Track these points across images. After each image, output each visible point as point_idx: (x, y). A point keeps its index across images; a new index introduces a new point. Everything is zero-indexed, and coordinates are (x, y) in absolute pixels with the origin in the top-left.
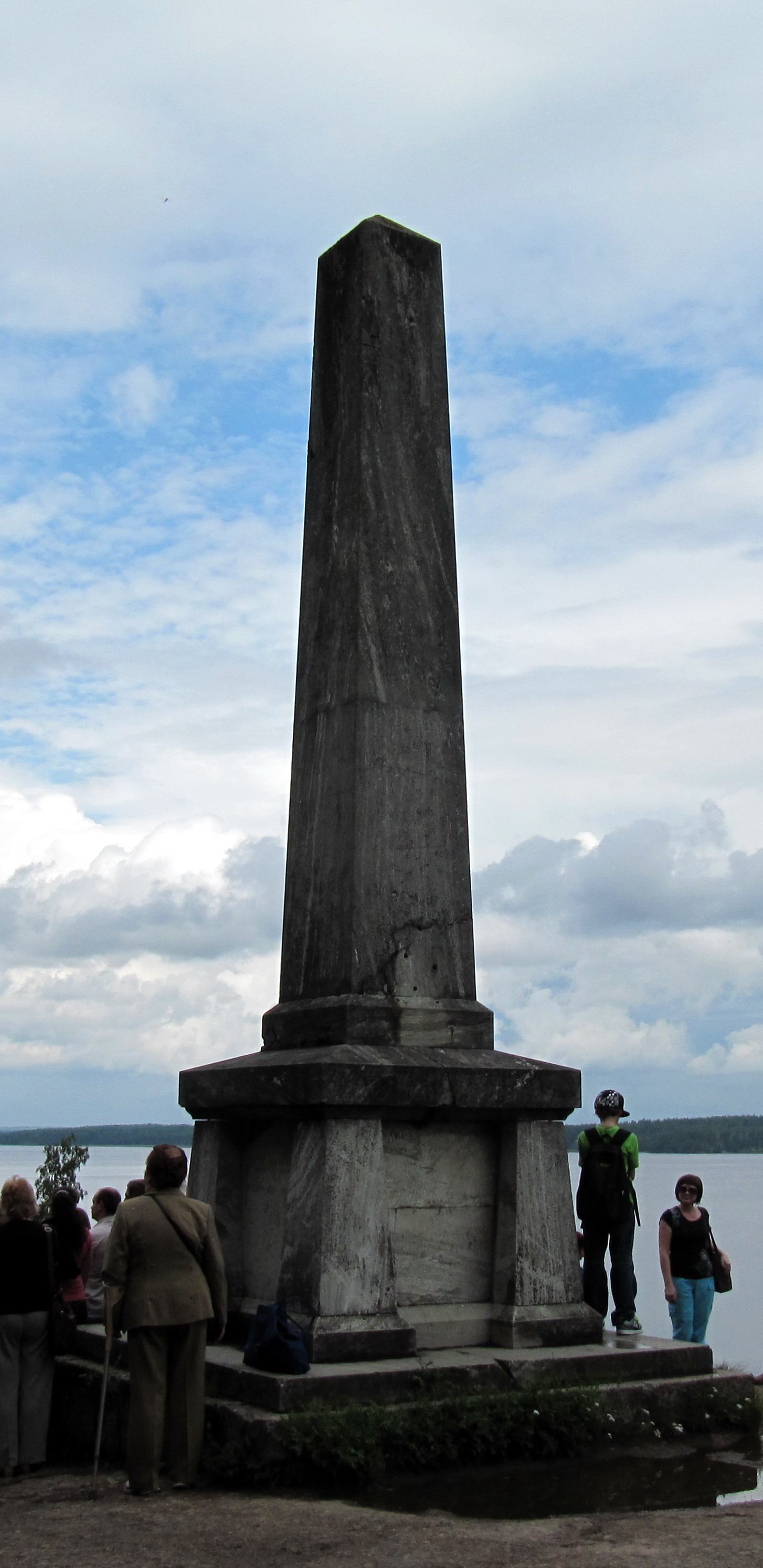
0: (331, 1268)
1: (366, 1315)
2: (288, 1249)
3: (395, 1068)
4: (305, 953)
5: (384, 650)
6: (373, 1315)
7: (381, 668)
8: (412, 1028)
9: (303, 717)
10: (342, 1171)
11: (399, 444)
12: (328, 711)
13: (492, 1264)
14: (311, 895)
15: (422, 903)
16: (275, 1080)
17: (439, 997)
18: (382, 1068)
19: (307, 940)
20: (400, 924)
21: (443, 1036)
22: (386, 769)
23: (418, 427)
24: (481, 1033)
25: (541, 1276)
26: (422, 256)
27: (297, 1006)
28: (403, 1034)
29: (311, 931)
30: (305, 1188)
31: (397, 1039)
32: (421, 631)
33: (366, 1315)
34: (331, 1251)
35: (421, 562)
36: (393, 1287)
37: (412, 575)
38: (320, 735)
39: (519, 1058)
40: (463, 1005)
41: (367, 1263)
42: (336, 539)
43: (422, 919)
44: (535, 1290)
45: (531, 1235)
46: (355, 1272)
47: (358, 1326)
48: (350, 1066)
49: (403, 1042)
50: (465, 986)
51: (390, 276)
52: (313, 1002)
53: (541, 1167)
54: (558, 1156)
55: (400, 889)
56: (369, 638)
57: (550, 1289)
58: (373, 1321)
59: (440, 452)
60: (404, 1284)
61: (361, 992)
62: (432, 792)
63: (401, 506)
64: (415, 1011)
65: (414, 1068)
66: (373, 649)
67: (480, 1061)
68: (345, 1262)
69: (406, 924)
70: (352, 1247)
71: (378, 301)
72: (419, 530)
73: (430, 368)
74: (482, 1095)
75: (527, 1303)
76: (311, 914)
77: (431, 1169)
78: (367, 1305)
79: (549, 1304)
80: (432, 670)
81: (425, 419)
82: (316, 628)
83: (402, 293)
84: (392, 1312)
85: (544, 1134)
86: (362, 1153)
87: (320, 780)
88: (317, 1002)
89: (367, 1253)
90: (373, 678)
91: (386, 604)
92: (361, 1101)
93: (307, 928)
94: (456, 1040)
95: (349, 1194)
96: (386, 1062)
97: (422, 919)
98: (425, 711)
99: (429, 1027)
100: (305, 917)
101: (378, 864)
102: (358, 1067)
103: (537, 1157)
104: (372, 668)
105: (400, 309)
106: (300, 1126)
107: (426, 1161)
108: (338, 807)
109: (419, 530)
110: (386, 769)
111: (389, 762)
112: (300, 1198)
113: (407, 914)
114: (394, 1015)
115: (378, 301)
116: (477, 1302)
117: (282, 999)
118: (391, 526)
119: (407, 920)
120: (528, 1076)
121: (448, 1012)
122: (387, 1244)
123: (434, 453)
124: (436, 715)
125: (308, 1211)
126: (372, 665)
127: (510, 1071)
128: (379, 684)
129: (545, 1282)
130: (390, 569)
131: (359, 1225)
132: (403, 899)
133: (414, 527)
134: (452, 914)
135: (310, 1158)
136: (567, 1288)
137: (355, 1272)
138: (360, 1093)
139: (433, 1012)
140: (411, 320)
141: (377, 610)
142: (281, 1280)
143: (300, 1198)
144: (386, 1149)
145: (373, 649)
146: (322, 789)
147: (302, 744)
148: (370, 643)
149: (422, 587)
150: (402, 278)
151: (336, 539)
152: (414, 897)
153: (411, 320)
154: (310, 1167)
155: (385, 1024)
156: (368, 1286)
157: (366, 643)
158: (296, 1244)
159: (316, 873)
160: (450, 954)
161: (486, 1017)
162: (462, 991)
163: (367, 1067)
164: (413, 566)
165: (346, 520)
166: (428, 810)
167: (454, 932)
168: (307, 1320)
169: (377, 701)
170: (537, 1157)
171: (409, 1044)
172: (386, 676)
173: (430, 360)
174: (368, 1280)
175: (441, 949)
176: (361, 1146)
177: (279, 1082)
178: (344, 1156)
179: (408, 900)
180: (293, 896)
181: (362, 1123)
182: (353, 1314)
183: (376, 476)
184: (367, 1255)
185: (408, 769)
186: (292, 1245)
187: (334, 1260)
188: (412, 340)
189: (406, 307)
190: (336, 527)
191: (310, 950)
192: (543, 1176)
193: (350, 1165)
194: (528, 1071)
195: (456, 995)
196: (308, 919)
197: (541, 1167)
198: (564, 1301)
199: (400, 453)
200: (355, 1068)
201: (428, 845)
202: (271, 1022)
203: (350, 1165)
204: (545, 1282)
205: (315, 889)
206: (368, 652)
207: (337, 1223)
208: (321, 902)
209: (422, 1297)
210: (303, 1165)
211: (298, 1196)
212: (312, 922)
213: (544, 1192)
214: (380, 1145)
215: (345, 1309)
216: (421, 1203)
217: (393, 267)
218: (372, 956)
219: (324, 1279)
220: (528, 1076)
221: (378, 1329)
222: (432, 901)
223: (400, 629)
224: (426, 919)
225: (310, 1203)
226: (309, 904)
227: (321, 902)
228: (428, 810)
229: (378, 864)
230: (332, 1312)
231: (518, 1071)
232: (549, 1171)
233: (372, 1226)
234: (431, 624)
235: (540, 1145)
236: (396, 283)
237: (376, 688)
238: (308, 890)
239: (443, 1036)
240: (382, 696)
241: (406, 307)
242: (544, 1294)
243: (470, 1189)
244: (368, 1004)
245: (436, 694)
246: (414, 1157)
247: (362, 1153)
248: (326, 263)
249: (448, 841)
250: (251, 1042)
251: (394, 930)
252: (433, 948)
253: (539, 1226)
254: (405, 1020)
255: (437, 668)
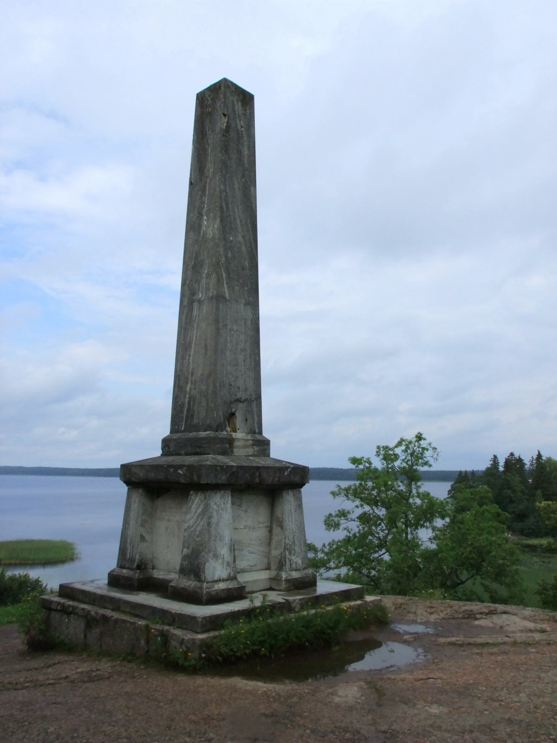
0: (210, 559)
1: (224, 580)
2: (185, 550)
3: (238, 466)
4: (185, 412)
5: (228, 276)
6: (227, 580)
7: (227, 283)
8: (238, 447)
9: (185, 303)
10: (215, 514)
11: (236, 182)
12: (199, 301)
13: (269, 552)
14: (189, 385)
15: (242, 391)
16: (179, 471)
17: (249, 433)
18: (232, 466)
19: (186, 406)
20: (233, 400)
21: (250, 451)
22: (228, 330)
23: (243, 176)
24: (266, 450)
25: (293, 557)
26: (247, 99)
27: (176, 436)
28: (235, 450)
29: (189, 402)
30: (195, 522)
31: (232, 452)
32: (243, 269)
33: (224, 580)
34: (210, 552)
35: (244, 237)
36: (235, 566)
37: (240, 243)
38: (195, 312)
39: (283, 461)
40: (258, 437)
41: (225, 556)
42: (205, 223)
43: (241, 398)
44: (291, 564)
45: (289, 540)
46: (220, 561)
47: (222, 586)
48: (220, 466)
49: (235, 454)
50: (258, 428)
51: (234, 106)
52: (191, 434)
53: (293, 510)
54: (299, 504)
55: (233, 384)
56: (222, 269)
57: (296, 563)
58: (228, 583)
59: (252, 189)
60: (242, 564)
61: (217, 431)
62: (246, 341)
63: (236, 210)
64: (239, 440)
65: (245, 466)
66: (224, 274)
67: (261, 462)
68: (216, 556)
69: (235, 400)
70: (218, 549)
71: (224, 120)
72: (243, 223)
73: (249, 150)
74: (272, 478)
75: (287, 570)
76: (189, 394)
77: (246, 511)
78: (224, 575)
79: (296, 570)
80: (247, 286)
81: (247, 173)
82: (193, 263)
83: (239, 114)
84: (234, 578)
85: (294, 495)
86: (223, 506)
87: (195, 333)
88: (193, 434)
89: (224, 551)
90: (224, 288)
91: (230, 255)
92: (224, 482)
93: (187, 400)
94: (256, 453)
95: (218, 524)
96: (234, 464)
97: (241, 398)
98: (245, 305)
99: (245, 447)
100: (186, 395)
101: (224, 373)
102: (223, 466)
103: (291, 505)
104: (223, 284)
105: (238, 122)
106: (191, 492)
107: (244, 508)
108: (206, 346)
109: (243, 223)
110: (228, 330)
111: (229, 327)
112: (192, 526)
113: (236, 396)
114: (231, 441)
115: (224, 120)
116: (263, 570)
117: (171, 433)
118: (232, 219)
119: (236, 398)
120: (289, 470)
121: (252, 440)
122: (233, 547)
123: (250, 189)
124: (248, 307)
125: (197, 533)
126: (223, 281)
127: (283, 467)
128: (226, 290)
129: (295, 561)
130: (231, 238)
131: (221, 540)
132: (234, 389)
133: (241, 221)
134: (254, 396)
135: (197, 509)
136: (302, 562)
137: (220, 561)
138: (223, 479)
139: (247, 440)
140: (242, 127)
141: (226, 257)
142: (181, 564)
143: (192, 526)
144: (233, 503)
145: (224, 274)
146: (196, 337)
147: (184, 316)
148: (223, 272)
149: (244, 249)
150: (239, 107)
151: (205, 223)
152: (239, 388)
153: (242, 127)
154: (198, 512)
155: (228, 446)
156: (225, 567)
157: (221, 272)
158: (190, 548)
159: (192, 376)
160: (253, 414)
161: (266, 444)
162: (257, 431)
163: (227, 466)
164: (240, 239)
165: (211, 215)
166: (245, 349)
167: (254, 404)
168: (198, 584)
169: (225, 298)
170: (291, 505)
171: (237, 455)
172: (229, 288)
173: (249, 147)
174: (225, 564)
175: (249, 411)
176: (222, 502)
177: (181, 472)
178: (215, 507)
179: (236, 389)
180: (178, 384)
181: (223, 492)
182: (219, 581)
183: (226, 195)
184: (224, 553)
185: (237, 330)
186: (188, 548)
187: (211, 556)
188: (242, 137)
189: (240, 120)
190: (205, 218)
191: (188, 410)
192: (293, 514)
193: (217, 511)
194: (289, 467)
195: (254, 433)
196: (188, 396)
197: (293, 510)
198: (301, 568)
199: (236, 186)
200: (222, 467)
201: (245, 365)
202: (166, 442)
203: (217, 511)
204: (295, 561)
205: (192, 383)
206: (222, 276)
207: (213, 538)
208: (195, 389)
209: (242, 569)
210: (194, 511)
211: (191, 525)
212: (190, 398)
213: (294, 520)
214: (230, 502)
215: (216, 578)
216: (242, 527)
217: (235, 103)
218: (221, 414)
219: (207, 564)
220: (289, 470)
221: (230, 587)
222: (246, 390)
223: (235, 266)
224: (243, 398)
225: (198, 529)
226: (188, 389)
227: (195, 389)
228: (245, 349)
229: (224, 373)
230: (211, 580)
231: (286, 467)
232: (296, 511)
233: (227, 540)
234: (247, 265)
235: (292, 500)
236: (236, 108)
237: (225, 293)
238: (187, 383)
239: (250, 451)
240: (228, 298)
241: (240, 120)
242: (294, 566)
243: (261, 519)
244: (220, 436)
245: (249, 297)
246: (239, 506)
247: (223, 506)
248: (201, 98)
249: (253, 364)
250: (157, 452)
251: (231, 403)
252: (246, 411)
253: (292, 536)
254: (236, 444)
255: (249, 286)
